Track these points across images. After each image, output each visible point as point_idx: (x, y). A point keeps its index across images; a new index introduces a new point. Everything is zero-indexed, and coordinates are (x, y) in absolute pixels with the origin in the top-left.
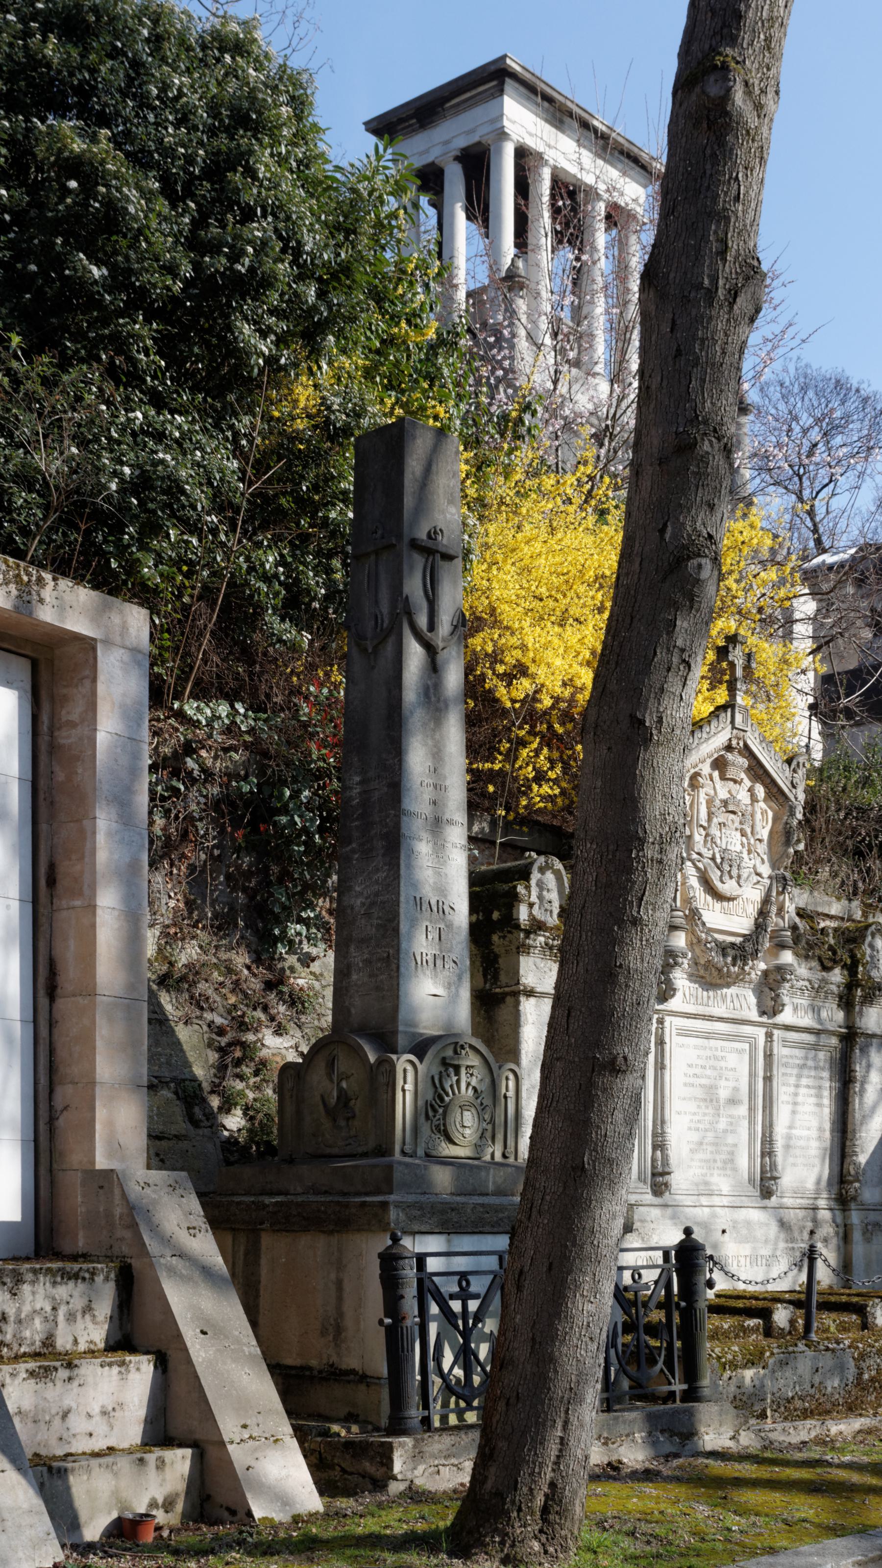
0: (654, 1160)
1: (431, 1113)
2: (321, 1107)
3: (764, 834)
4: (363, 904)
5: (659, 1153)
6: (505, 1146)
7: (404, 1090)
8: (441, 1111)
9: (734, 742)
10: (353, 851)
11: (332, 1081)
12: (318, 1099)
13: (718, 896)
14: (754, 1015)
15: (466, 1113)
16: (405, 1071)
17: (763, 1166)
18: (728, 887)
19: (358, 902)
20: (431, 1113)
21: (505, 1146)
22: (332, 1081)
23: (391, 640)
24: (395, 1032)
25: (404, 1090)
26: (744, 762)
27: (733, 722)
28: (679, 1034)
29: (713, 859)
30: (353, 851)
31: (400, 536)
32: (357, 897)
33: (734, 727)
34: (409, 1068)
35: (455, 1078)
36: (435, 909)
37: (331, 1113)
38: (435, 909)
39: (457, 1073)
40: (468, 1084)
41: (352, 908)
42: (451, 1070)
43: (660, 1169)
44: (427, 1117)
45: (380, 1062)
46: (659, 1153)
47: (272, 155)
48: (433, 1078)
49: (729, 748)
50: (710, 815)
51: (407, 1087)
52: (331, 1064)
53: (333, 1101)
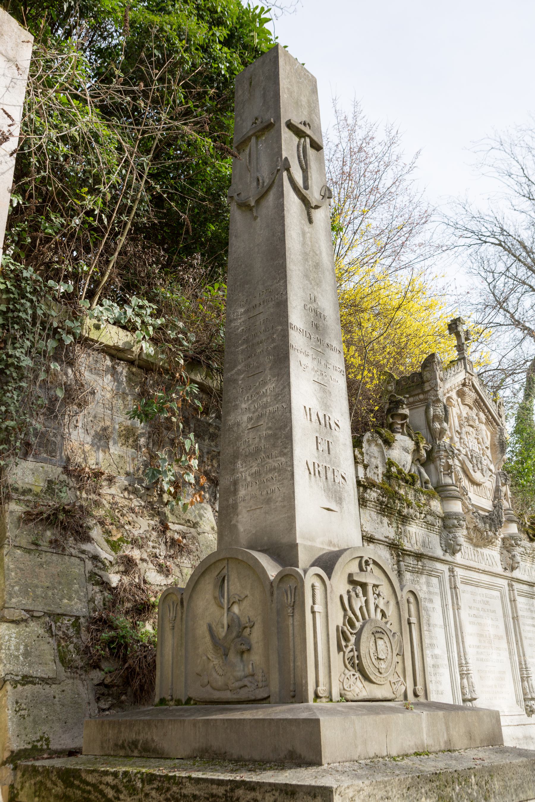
0: (463, 688)
1: (343, 643)
2: (208, 639)
3: (488, 444)
4: (250, 419)
5: (465, 681)
6: (415, 684)
7: (313, 612)
8: (353, 639)
9: (467, 381)
10: (239, 373)
11: (221, 607)
12: (205, 628)
13: (473, 482)
14: (499, 569)
15: (380, 642)
16: (313, 586)
17: (524, 689)
18: (477, 476)
19: (245, 418)
20: (343, 643)
21: (415, 684)
22: (221, 607)
23: (271, 197)
24: (294, 546)
25: (313, 612)
26: (474, 395)
27: (465, 368)
28: (462, 582)
29: (466, 455)
30: (239, 373)
31: (278, 118)
32: (243, 414)
33: (467, 372)
34: (318, 584)
35: (363, 599)
36: (322, 422)
37: (221, 647)
38: (322, 422)
39: (365, 594)
40: (377, 607)
41: (238, 425)
42: (359, 589)
43: (468, 696)
44: (340, 649)
45: (282, 578)
46: (465, 681)
47: (153, 121)
48: (341, 597)
49: (464, 385)
50: (461, 426)
51: (317, 608)
52: (221, 582)
53: (222, 633)
